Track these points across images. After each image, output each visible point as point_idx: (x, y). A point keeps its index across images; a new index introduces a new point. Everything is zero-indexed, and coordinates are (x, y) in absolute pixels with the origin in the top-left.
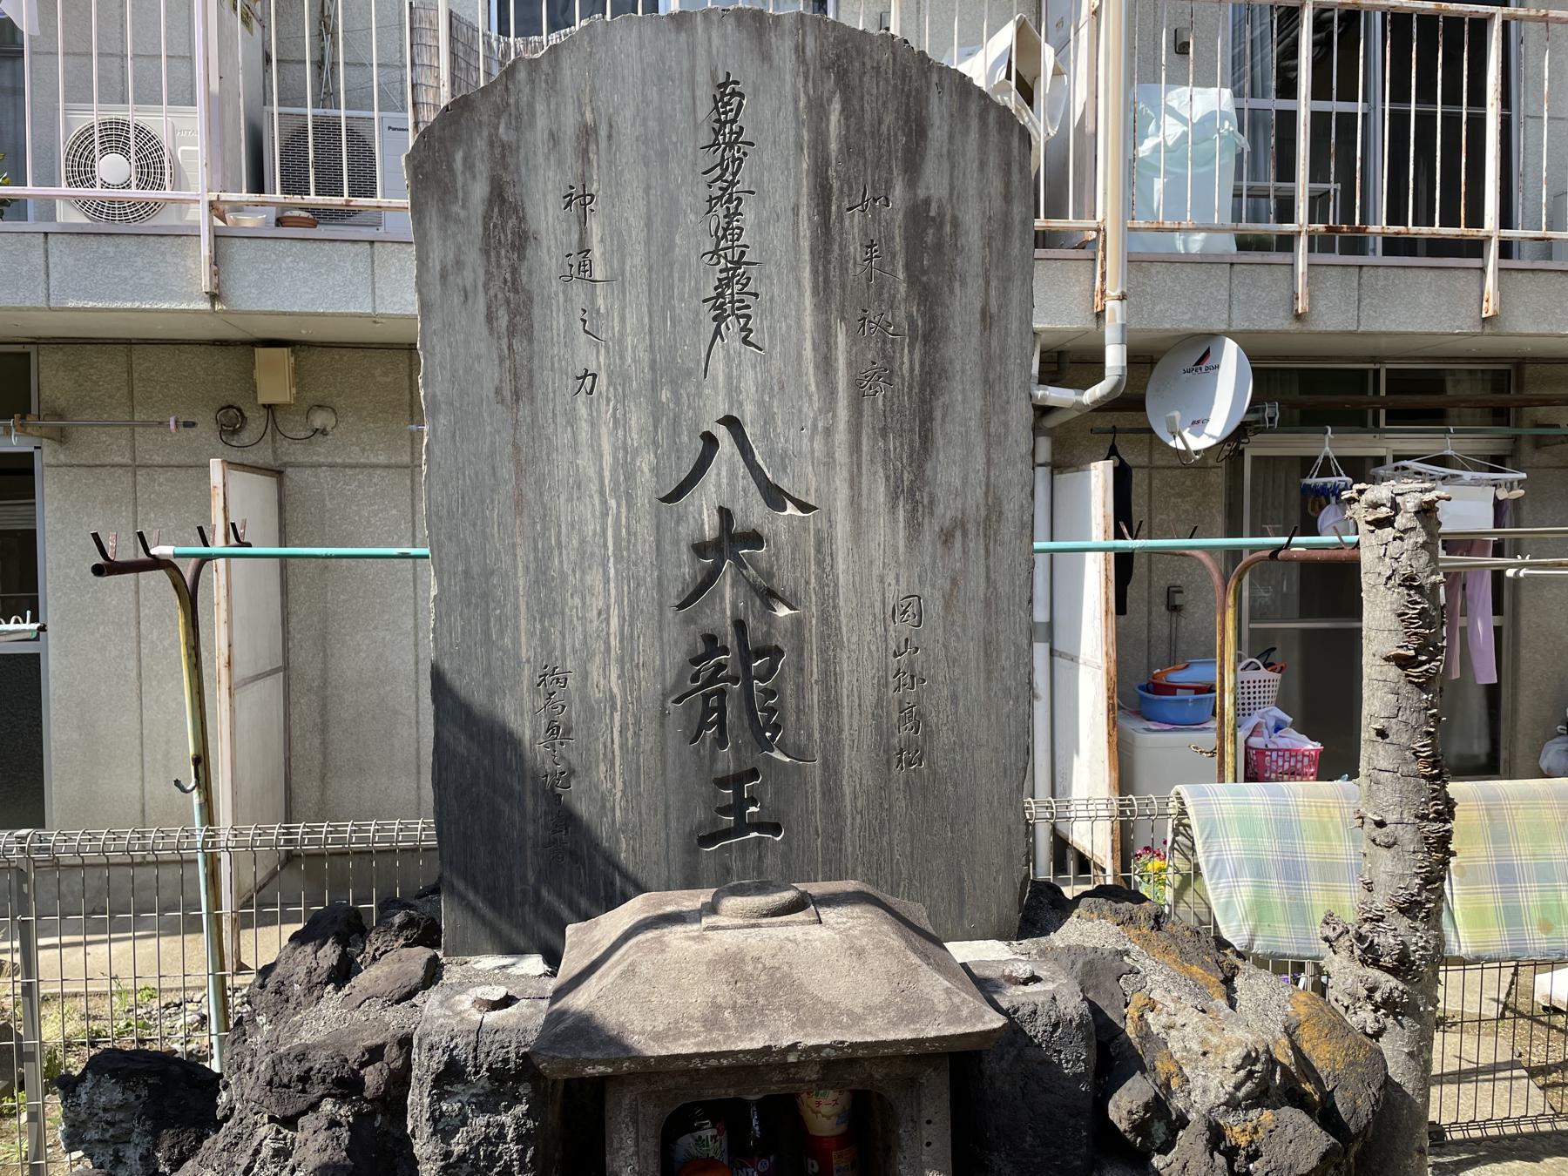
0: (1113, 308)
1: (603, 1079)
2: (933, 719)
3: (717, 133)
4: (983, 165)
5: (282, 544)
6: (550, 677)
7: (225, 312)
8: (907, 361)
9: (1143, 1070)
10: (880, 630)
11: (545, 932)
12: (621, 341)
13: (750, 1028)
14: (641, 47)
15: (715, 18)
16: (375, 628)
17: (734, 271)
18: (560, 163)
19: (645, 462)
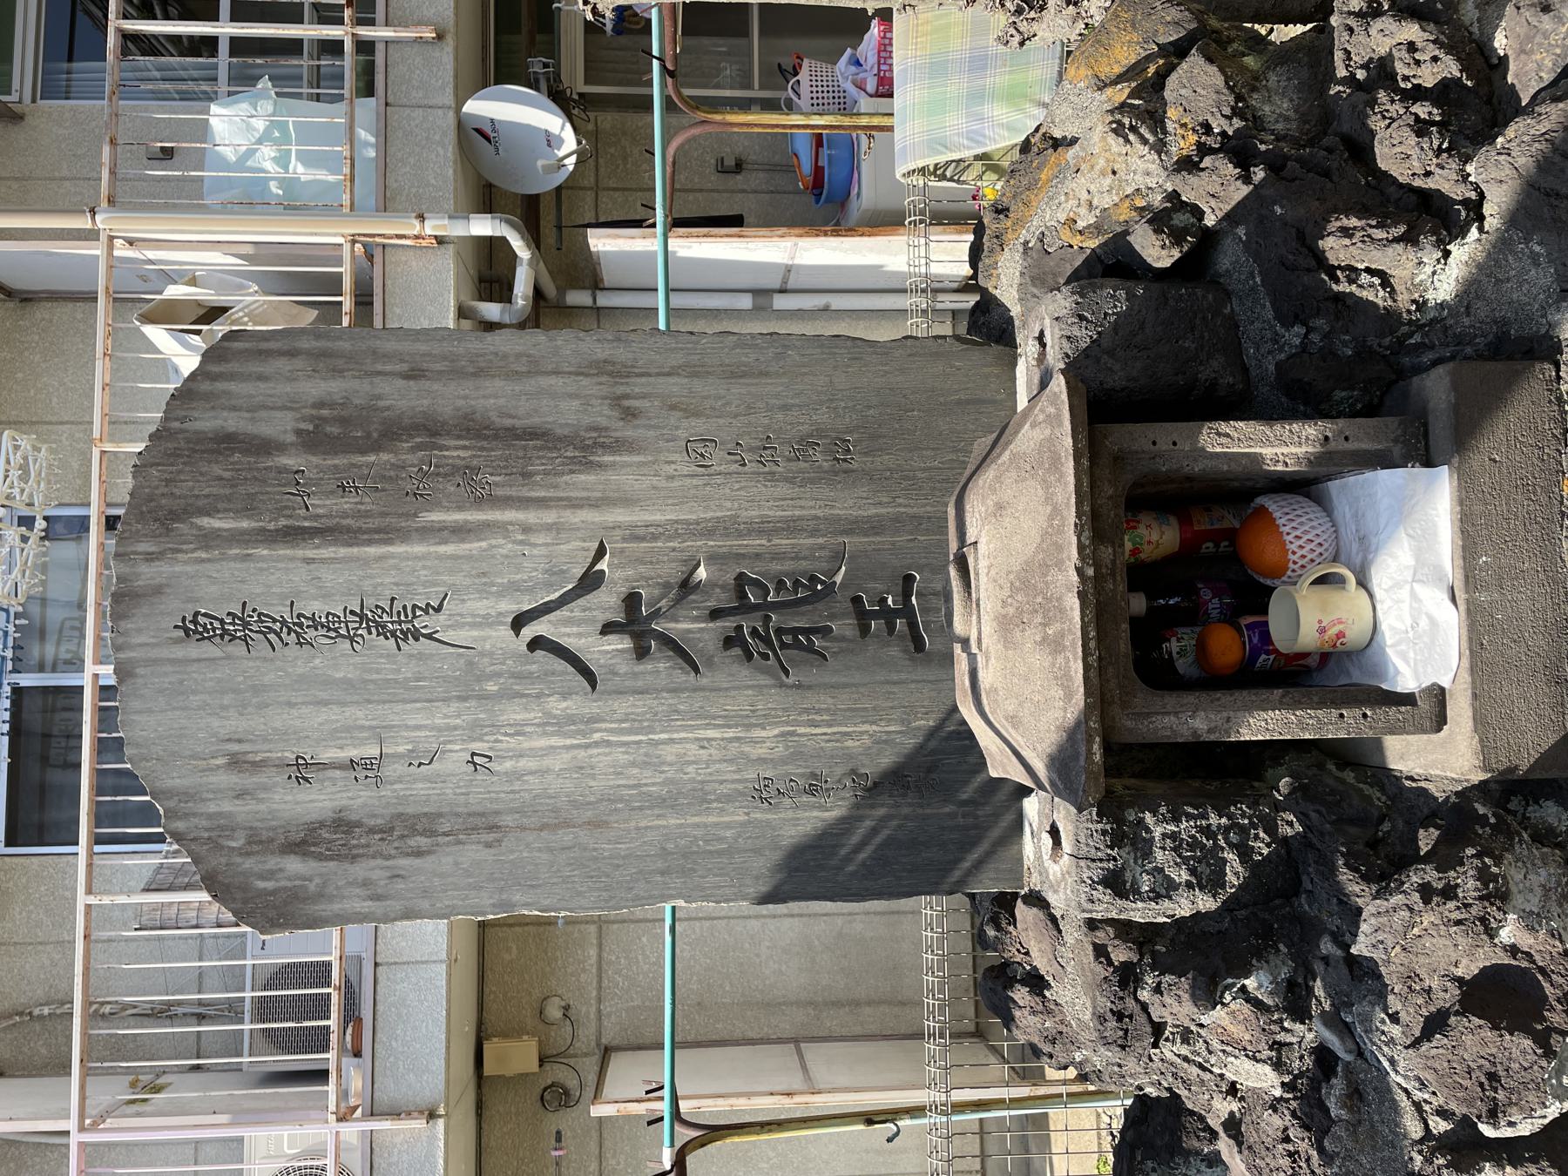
0: (431, 227)
1: (1107, 748)
2: (805, 429)
3: (234, 638)
4: (261, 378)
5: (661, 1047)
6: (763, 793)
7: (447, 1105)
8: (456, 452)
9: (1126, 233)
10: (719, 480)
11: (1001, 796)
12: (439, 729)
13: (1062, 611)
14: (150, 711)
15: (121, 640)
16: (758, 955)
17: (368, 620)
18: (265, 788)
19: (557, 705)
